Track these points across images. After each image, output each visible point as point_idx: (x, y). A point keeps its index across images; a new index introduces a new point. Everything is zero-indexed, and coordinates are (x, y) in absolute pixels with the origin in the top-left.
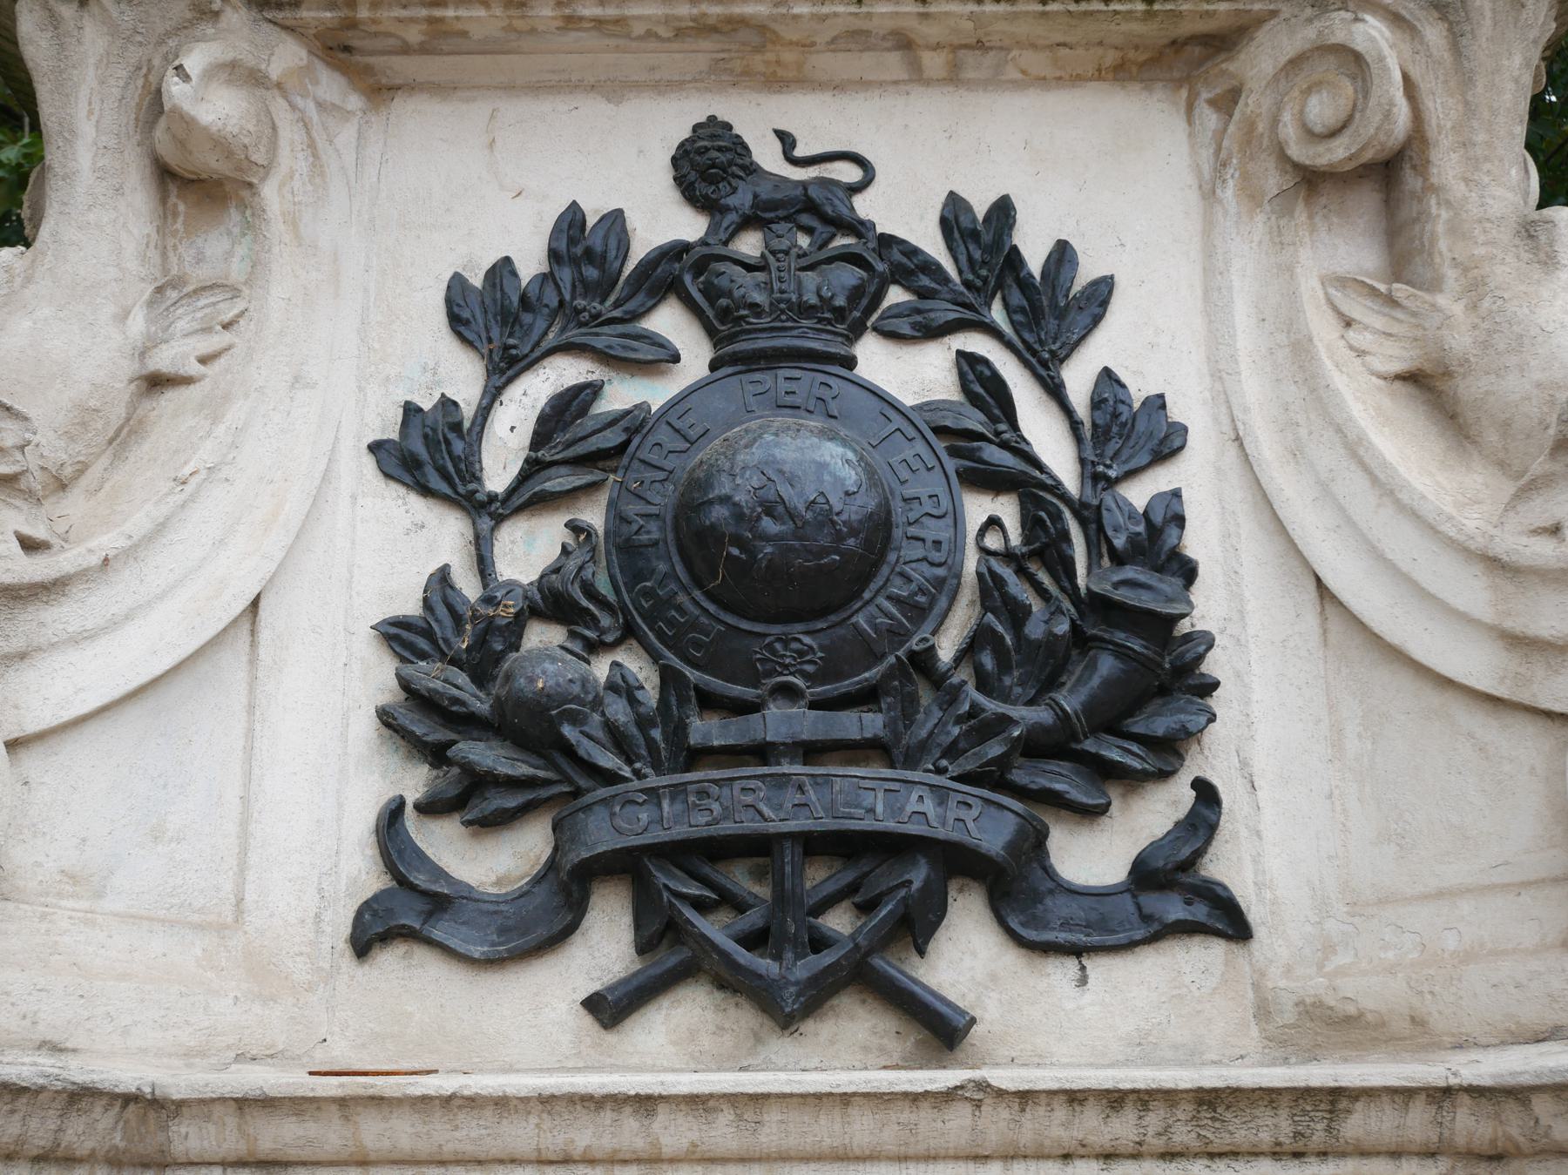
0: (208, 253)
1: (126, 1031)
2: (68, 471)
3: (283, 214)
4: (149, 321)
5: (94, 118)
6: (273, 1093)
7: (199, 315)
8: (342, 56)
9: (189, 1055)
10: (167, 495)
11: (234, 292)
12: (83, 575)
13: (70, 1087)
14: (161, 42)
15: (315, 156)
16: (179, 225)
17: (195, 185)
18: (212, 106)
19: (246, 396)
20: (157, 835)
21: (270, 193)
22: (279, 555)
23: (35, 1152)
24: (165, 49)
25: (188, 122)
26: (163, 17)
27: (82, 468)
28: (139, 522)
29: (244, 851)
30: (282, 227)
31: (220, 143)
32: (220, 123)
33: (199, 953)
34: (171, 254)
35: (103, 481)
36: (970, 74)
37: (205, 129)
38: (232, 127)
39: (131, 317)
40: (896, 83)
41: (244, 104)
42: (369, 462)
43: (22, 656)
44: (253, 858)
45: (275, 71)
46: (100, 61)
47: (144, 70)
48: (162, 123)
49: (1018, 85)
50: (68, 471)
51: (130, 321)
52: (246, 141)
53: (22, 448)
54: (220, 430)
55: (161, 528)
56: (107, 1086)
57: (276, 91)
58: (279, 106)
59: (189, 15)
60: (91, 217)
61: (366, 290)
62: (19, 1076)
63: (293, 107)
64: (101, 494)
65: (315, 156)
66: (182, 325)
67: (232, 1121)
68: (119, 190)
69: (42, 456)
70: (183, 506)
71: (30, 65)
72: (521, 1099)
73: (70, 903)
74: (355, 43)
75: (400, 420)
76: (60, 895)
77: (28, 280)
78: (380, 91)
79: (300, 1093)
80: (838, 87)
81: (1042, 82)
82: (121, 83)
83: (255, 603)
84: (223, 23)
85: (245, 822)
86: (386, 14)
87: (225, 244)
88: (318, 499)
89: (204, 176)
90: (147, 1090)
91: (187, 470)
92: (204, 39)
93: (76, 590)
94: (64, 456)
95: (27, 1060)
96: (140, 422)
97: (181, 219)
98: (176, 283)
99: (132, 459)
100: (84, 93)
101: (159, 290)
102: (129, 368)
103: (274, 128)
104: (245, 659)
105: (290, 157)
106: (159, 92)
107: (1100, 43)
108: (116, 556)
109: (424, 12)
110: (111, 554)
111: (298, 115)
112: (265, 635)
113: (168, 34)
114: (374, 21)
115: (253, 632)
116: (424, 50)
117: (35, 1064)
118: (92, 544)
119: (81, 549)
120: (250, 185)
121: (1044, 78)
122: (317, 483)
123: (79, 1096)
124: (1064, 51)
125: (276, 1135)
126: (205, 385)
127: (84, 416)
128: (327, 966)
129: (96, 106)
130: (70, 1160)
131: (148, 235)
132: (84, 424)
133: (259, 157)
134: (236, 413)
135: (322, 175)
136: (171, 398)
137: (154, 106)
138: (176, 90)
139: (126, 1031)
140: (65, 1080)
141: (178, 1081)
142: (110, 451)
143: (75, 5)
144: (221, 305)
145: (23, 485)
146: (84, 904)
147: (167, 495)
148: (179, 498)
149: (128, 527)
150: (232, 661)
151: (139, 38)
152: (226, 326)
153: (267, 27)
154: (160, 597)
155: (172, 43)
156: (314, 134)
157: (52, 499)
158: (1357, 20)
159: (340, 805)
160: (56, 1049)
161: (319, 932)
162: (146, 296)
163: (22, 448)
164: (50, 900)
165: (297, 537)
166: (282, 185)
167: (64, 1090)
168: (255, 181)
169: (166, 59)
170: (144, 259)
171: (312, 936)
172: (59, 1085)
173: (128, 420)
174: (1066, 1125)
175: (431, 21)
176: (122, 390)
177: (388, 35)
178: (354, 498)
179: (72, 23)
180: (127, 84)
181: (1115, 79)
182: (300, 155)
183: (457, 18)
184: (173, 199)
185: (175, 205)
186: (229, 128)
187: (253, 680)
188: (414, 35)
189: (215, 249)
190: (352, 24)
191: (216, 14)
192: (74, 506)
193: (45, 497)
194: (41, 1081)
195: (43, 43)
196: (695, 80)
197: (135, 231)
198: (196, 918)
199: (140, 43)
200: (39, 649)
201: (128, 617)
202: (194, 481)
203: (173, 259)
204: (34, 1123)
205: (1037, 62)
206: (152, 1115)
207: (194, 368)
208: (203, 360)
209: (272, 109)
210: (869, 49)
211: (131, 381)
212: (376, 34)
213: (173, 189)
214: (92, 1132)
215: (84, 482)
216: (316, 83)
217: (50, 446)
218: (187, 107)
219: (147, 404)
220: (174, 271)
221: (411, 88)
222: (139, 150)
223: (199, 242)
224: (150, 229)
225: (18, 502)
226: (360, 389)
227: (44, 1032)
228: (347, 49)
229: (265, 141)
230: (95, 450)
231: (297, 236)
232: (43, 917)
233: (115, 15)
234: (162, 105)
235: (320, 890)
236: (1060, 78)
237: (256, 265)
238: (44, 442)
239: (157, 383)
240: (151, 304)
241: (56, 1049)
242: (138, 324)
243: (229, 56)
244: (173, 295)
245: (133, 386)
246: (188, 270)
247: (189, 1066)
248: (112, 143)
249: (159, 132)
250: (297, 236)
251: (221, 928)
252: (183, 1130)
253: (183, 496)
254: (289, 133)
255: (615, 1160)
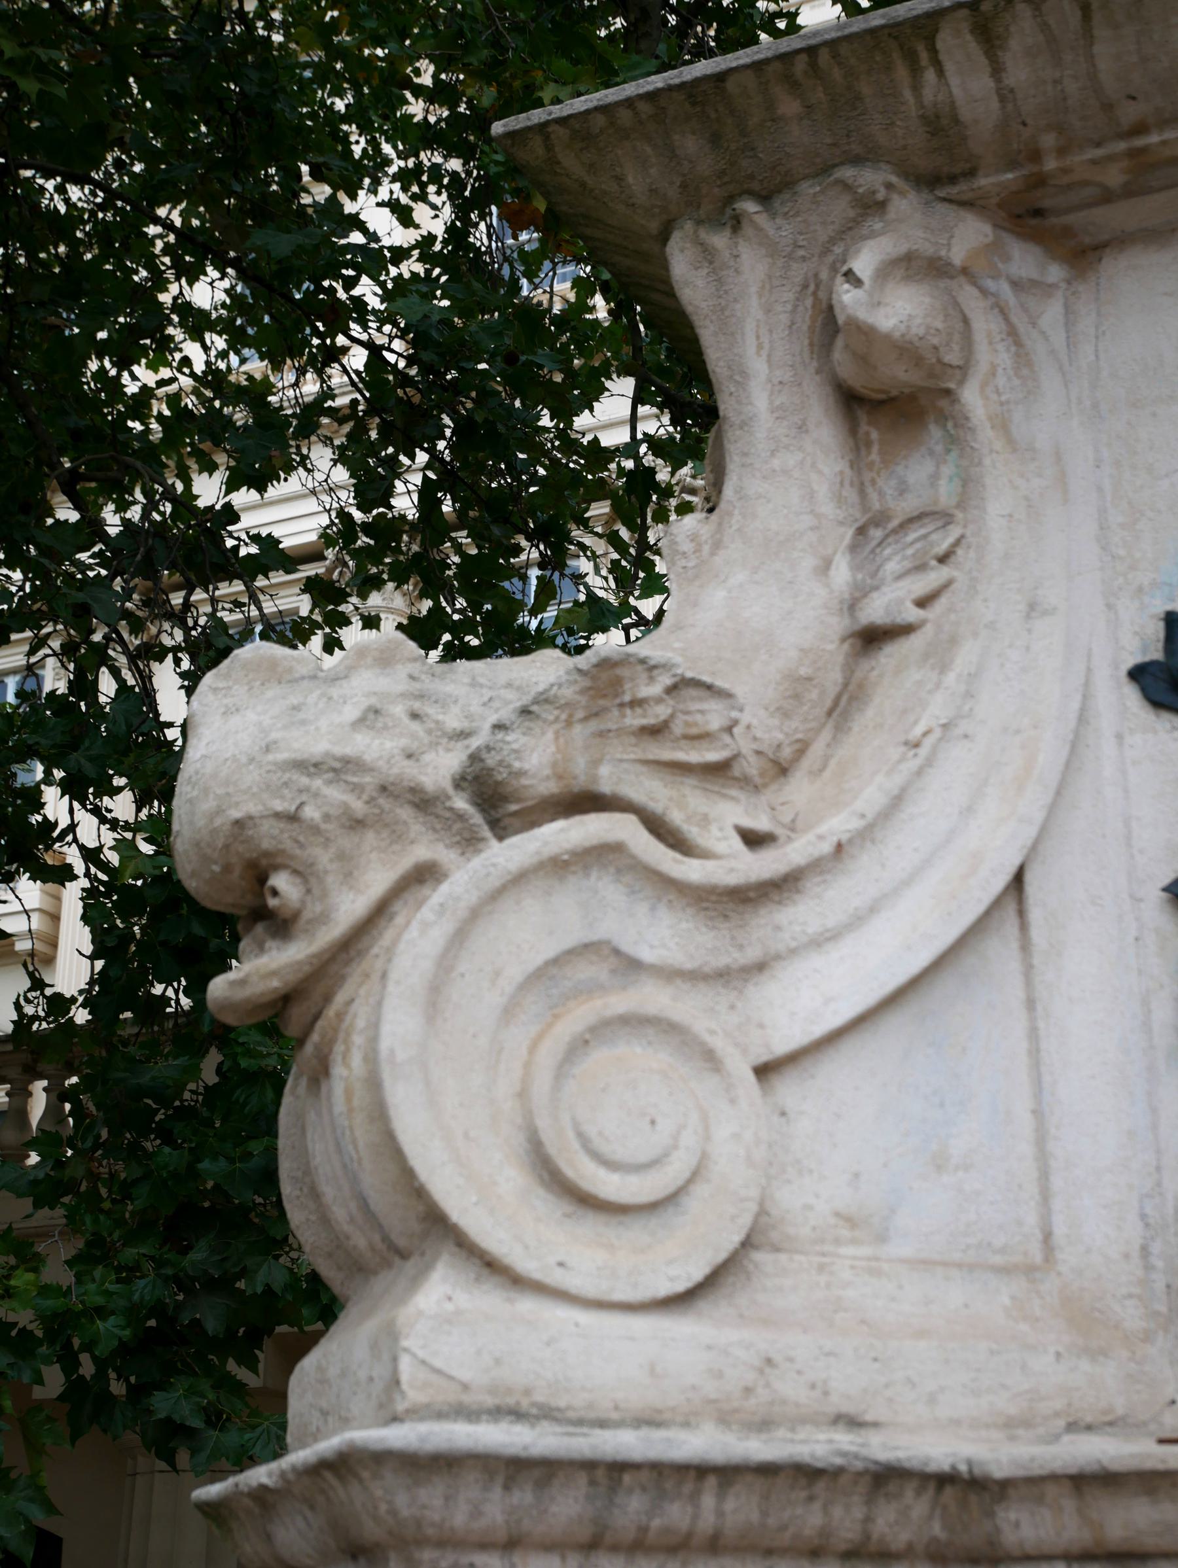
0: (911, 479)
1: (932, 1399)
2: (787, 753)
3: (990, 418)
4: (855, 568)
5: (764, 353)
6: (1115, 1467)
7: (910, 552)
8: (1033, 222)
9: (1011, 1425)
10: (900, 761)
11: (945, 518)
12: (815, 867)
13: (872, 1467)
14: (826, 251)
15: (1018, 343)
16: (874, 456)
17: (888, 406)
18: (896, 310)
19: (975, 635)
20: (940, 1163)
21: (972, 397)
22: (1039, 816)
23: (843, 1547)
24: (830, 259)
25: (866, 333)
26: (824, 223)
27: (802, 748)
28: (871, 797)
29: (1044, 1176)
30: (990, 433)
31: (906, 349)
32: (903, 327)
33: (1007, 1301)
34: (869, 490)
35: (826, 759)
37: (887, 337)
38: (917, 330)
39: (833, 567)
41: (927, 300)
42: (1132, 695)
43: (761, 967)
44: (1057, 1182)
45: (957, 256)
46: (763, 287)
47: (812, 287)
48: (840, 342)
50: (787, 753)
51: (832, 572)
52: (935, 341)
53: (729, 730)
54: (951, 678)
55: (897, 801)
56: (915, 1464)
57: (962, 279)
58: (969, 297)
59: (851, 213)
60: (776, 463)
61: (1100, 489)
62: (812, 1456)
63: (984, 292)
64: (827, 774)
65: (1018, 343)
66: (892, 567)
67: (1069, 1504)
68: (802, 428)
69: (755, 739)
70: (919, 773)
71: (689, 309)
73: (849, 1251)
74: (1046, 203)
75: (1162, 634)
76: (837, 1241)
77: (717, 545)
78: (1082, 254)
79: (1149, 1465)
82: (789, 307)
83: (1018, 880)
84: (892, 212)
85: (1041, 1139)
86: (1077, 159)
87: (928, 466)
88: (1075, 746)
89: (894, 393)
90: (963, 1468)
91: (918, 730)
92: (872, 235)
93: (811, 885)
94: (780, 736)
95: (822, 1437)
96: (860, 686)
97: (875, 448)
98: (879, 519)
99: (856, 729)
100: (750, 327)
101: (861, 531)
102: (838, 625)
103: (966, 321)
104: (1015, 945)
105: (990, 352)
106: (831, 308)
108: (850, 841)
109: (1122, 146)
110: (844, 838)
111: (992, 300)
112: (1035, 914)
113: (832, 241)
114: (1065, 171)
115: (1021, 913)
116: (1129, 192)
117: (831, 1441)
118: (823, 829)
119: (810, 836)
120: (948, 392)
122: (1072, 724)
123: (885, 1478)
125: (1128, 1520)
126: (928, 631)
127: (796, 687)
128: (1163, 1309)
129: (765, 339)
130: (885, 1555)
131: (841, 473)
132: (797, 697)
133: (952, 357)
134: (966, 657)
135: (1029, 364)
136: (891, 654)
137: (828, 326)
138: (848, 298)
139: (932, 1399)
140: (865, 1459)
141: (1000, 1456)
142: (830, 725)
143: (727, 232)
144: (934, 537)
145: (736, 771)
146: (865, 1251)
147: (900, 761)
148: (912, 765)
149: (859, 805)
150: (1001, 950)
151: (801, 252)
152: (943, 559)
153: (942, 208)
154: (908, 882)
155: (838, 250)
156: (1014, 320)
157: (774, 787)
159: (1154, 1110)
160: (853, 1423)
161: (1148, 1268)
162: (847, 540)
163: (729, 730)
164: (827, 1248)
165: (1058, 793)
166: (983, 386)
167: (866, 1472)
168: (952, 385)
169: (834, 269)
170: (840, 500)
171: (1140, 1273)
172: (859, 1465)
173: (846, 685)
175: (1133, 153)
176: (835, 651)
177: (1085, 183)
178: (1119, 737)
179: (727, 254)
180: (795, 307)
182: (1000, 347)
183: (1164, 143)
184: (864, 428)
185: (867, 434)
186: (914, 330)
187: (1028, 970)
188: (1114, 177)
189: (921, 476)
190: (1039, 181)
191: (882, 205)
192: (799, 791)
193: (765, 786)
194: (838, 1461)
195: (700, 283)
197: (826, 470)
198: (998, 1260)
199: (804, 259)
200: (778, 957)
201: (874, 909)
202: (928, 743)
203: (873, 496)
204: (837, 1512)
206: (973, 1498)
207: (912, 614)
208: (922, 603)
209: (960, 299)
211: (843, 640)
212: (1069, 187)
213: (862, 416)
214: (902, 1522)
215: (806, 763)
216: (1007, 259)
217: (759, 725)
218: (862, 314)
219: (865, 664)
220: (877, 506)
221: (1121, 241)
222: (818, 378)
223: (899, 469)
224: (842, 465)
225: (734, 792)
226: (1109, 606)
227: (838, 1403)
228: (1038, 213)
229: (957, 337)
230: (813, 724)
231: (1011, 442)
232: (821, 1268)
233: (771, 232)
234: (835, 322)
235: (1143, 1216)
237: (969, 487)
238: (755, 722)
239: (872, 638)
240: (854, 548)
241: (853, 1423)
242: (842, 573)
243: (903, 249)
244: (877, 534)
245: (846, 646)
246: (891, 504)
247: (1012, 1439)
248: (788, 376)
249: (838, 354)
250: (1011, 442)
251: (1029, 1270)
252: (1013, 1516)
253: (918, 762)
254: (984, 324)
255: (715, 1545)
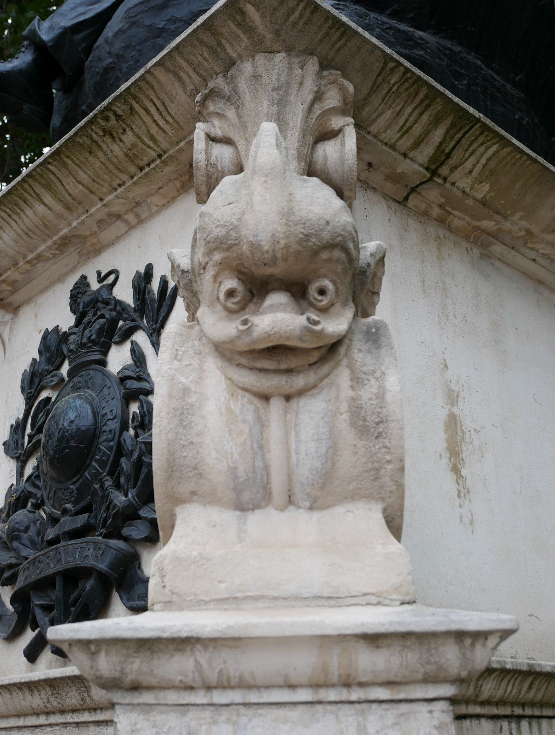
36: (143, 217)
40: (126, 232)
49: (158, 212)
72: (373, 498)
80: (112, 244)
81: (164, 207)
93: (242, 386)
107: (170, 180)
121: (164, 205)
124: (161, 190)
158: (68, 176)
174: (35, 721)
181: (185, 191)
196: (78, 263)
205: (157, 200)
210: (110, 225)
236: (168, 202)
